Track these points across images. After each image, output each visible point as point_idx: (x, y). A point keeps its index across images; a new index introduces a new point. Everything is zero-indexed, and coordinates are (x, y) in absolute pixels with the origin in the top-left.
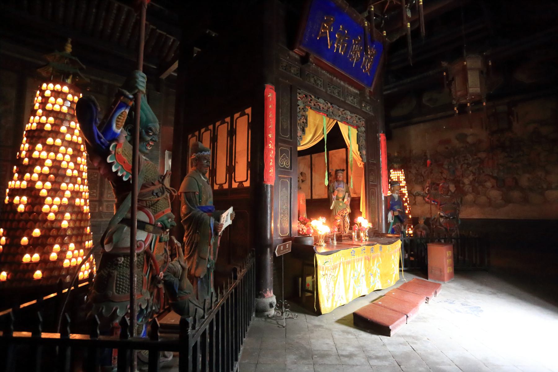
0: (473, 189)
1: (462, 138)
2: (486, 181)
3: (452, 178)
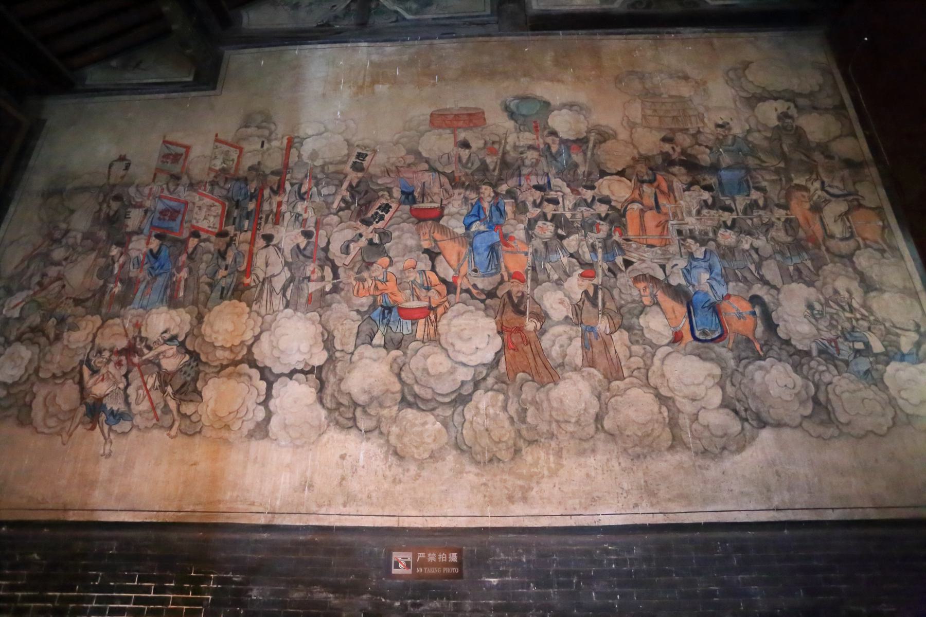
0: (586, 346)
1: (528, 113)
2: (643, 310)
3: (484, 283)
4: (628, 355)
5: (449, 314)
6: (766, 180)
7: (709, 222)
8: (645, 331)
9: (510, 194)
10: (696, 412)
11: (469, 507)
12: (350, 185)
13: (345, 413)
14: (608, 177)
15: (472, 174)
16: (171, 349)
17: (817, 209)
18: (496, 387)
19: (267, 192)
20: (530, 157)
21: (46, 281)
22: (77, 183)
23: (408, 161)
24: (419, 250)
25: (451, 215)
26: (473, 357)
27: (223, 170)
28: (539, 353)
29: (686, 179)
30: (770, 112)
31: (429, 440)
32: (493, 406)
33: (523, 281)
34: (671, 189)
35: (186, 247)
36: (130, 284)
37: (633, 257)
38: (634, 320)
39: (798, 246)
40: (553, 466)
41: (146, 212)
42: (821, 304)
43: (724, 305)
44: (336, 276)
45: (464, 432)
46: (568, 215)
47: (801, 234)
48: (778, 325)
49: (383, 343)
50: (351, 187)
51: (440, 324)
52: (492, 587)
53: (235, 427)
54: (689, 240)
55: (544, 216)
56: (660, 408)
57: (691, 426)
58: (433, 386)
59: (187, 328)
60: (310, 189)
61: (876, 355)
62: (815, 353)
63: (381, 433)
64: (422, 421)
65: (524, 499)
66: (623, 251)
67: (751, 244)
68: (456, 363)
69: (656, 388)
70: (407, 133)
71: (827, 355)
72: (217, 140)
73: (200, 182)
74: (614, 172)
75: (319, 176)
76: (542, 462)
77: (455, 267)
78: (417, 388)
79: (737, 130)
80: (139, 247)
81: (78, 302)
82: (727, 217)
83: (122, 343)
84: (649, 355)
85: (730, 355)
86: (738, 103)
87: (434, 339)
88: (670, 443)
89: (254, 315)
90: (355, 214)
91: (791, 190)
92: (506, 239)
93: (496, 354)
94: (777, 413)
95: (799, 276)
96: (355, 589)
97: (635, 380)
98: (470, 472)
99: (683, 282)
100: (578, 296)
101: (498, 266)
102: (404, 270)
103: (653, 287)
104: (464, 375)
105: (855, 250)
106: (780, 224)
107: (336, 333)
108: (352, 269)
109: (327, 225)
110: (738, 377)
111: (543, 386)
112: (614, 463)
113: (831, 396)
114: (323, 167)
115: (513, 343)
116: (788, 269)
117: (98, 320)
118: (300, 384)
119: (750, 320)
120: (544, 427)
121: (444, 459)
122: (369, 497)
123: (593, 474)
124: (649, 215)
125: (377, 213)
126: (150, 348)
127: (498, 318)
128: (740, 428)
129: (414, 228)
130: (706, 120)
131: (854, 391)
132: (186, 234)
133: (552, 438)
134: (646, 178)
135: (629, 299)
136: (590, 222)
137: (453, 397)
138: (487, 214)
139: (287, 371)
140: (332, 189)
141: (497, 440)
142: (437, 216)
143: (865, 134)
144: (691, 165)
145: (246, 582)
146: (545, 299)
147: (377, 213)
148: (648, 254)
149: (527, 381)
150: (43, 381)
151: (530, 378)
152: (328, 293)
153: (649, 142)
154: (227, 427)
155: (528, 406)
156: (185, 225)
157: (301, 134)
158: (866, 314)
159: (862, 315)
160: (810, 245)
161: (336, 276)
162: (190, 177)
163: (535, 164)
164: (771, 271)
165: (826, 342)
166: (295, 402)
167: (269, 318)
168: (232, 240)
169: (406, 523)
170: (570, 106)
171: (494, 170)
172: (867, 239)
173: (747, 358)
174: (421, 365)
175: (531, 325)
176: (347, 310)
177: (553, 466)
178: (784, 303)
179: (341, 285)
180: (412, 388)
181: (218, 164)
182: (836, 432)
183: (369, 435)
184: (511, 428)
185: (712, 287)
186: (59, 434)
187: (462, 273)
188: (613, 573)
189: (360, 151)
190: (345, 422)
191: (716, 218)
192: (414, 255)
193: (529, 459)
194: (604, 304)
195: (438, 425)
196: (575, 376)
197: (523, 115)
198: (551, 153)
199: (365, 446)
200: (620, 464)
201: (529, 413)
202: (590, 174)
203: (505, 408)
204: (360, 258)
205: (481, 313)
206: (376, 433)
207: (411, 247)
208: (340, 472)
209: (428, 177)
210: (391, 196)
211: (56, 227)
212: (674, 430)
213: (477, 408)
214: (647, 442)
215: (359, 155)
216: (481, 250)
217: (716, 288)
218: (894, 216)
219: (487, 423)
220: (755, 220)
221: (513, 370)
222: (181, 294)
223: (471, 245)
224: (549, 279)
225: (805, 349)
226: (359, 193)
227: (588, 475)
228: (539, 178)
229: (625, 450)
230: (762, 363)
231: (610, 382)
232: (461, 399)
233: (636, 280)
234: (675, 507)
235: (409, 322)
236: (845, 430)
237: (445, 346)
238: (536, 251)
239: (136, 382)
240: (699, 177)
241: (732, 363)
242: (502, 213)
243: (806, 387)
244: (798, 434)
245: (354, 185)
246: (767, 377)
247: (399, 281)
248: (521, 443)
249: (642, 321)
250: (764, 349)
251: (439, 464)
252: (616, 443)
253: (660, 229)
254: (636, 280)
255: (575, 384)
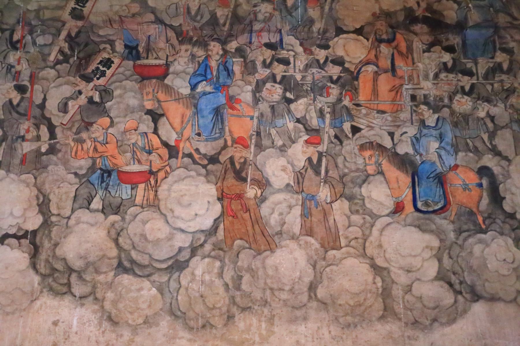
0: (306, 214)
2: (366, 179)
3: (207, 148)
4: (347, 224)
5: (170, 179)
6: (515, 41)
7: (446, 88)
8: (367, 201)
9: (240, 52)
10: (409, 283)
12: (69, 35)
14: (345, 36)
15: (201, 28)
18: (213, 254)
20: (263, 11)
24: (141, 111)
25: (177, 74)
26: (191, 224)
28: (257, 221)
29: (428, 39)
31: (144, 306)
32: (209, 273)
33: (247, 147)
34: (410, 49)
37: (361, 123)
38: (356, 190)
40: (264, 332)
43: (451, 175)
44: (52, 135)
45: (179, 298)
46: (298, 77)
49: (101, 208)
50: (69, 38)
51: (160, 189)
54: (423, 107)
55: (273, 78)
56: (375, 278)
57: (403, 298)
58: (151, 252)
60: (23, 37)
63: (96, 299)
64: (138, 287)
66: (351, 117)
67: (488, 113)
68: (175, 229)
69: (372, 259)
74: (352, 29)
76: (253, 329)
77: (178, 129)
78: (134, 254)
82: (466, 82)
84: (368, 225)
85: (451, 227)
87: (154, 204)
88: (381, 313)
90: (74, 69)
93: (215, 220)
94: (492, 287)
97: (352, 250)
98: (183, 337)
99: (411, 151)
100: (301, 163)
101: (222, 129)
102: (125, 132)
103: (379, 155)
104: (182, 241)
107: (51, 197)
108: (70, 129)
109: (43, 79)
110: (456, 250)
111: (260, 254)
114: (37, 11)
115: (232, 210)
118: (12, 249)
119: (475, 193)
120: (258, 295)
121: (157, 325)
123: (303, 341)
124: (383, 78)
125: (98, 68)
127: (219, 184)
128: (452, 301)
129: (137, 86)
133: (265, 306)
134: (384, 37)
135: (353, 167)
136: (320, 84)
137: (170, 263)
138: (215, 73)
140: (49, 39)
141: (211, 306)
142: (162, 73)
144: (435, 23)
146: (267, 166)
147: (98, 68)
148: (377, 121)
149: (244, 248)
151: (247, 245)
152: (44, 154)
155: (244, 273)
161: (52, 135)
163: (268, 19)
164: (504, 142)
166: (7, 268)
171: (224, 25)
173: (467, 231)
174: (139, 231)
175: (251, 192)
176: (65, 172)
177: (264, 332)
179: (58, 146)
180: (129, 254)
183: (84, 301)
184: (225, 294)
185: (440, 156)
187: (186, 136)
190: (60, 288)
191: (454, 83)
192: (137, 116)
193: (242, 325)
194: (327, 172)
195: (154, 291)
196: (293, 245)
198: (286, 6)
199: (79, 311)
200: (330, 332)
202: (325, 31)
203: (221, 275)
204: (78, 117)
205: (203, 179)
206: (91, 298)
207: (134, 108)
208: (52, 338)
209: (153, 30)
210: (113, 50)
213: (193, 274)
214: (358, 311)
216: (206, 113)
217: (444, 157)
219: (202, 289)
220: (496, 85)
221: (230, 238)
223: (196, 106)
224: (273, 145)
226: (78, 45)
227: (298, 342)
228: (272, 34)
229: (336, 318)
230: (483, 236)
232: (178, 265)
233: (362, 147)
235: (129, 186)
237: (164, 212)
238: (262, 115)
240: (442, 37)
241: (452, 236)
242: (230, 73)
244: (511, 309)
245: (73, 35)
246: (487, 250)
247: (119, 144)
248: (234, 309)
249: (364, 190)
250: (486, 223)
251: (153, 330)
253: (393, 93)
254: (362, 147)
255: (291, 253)
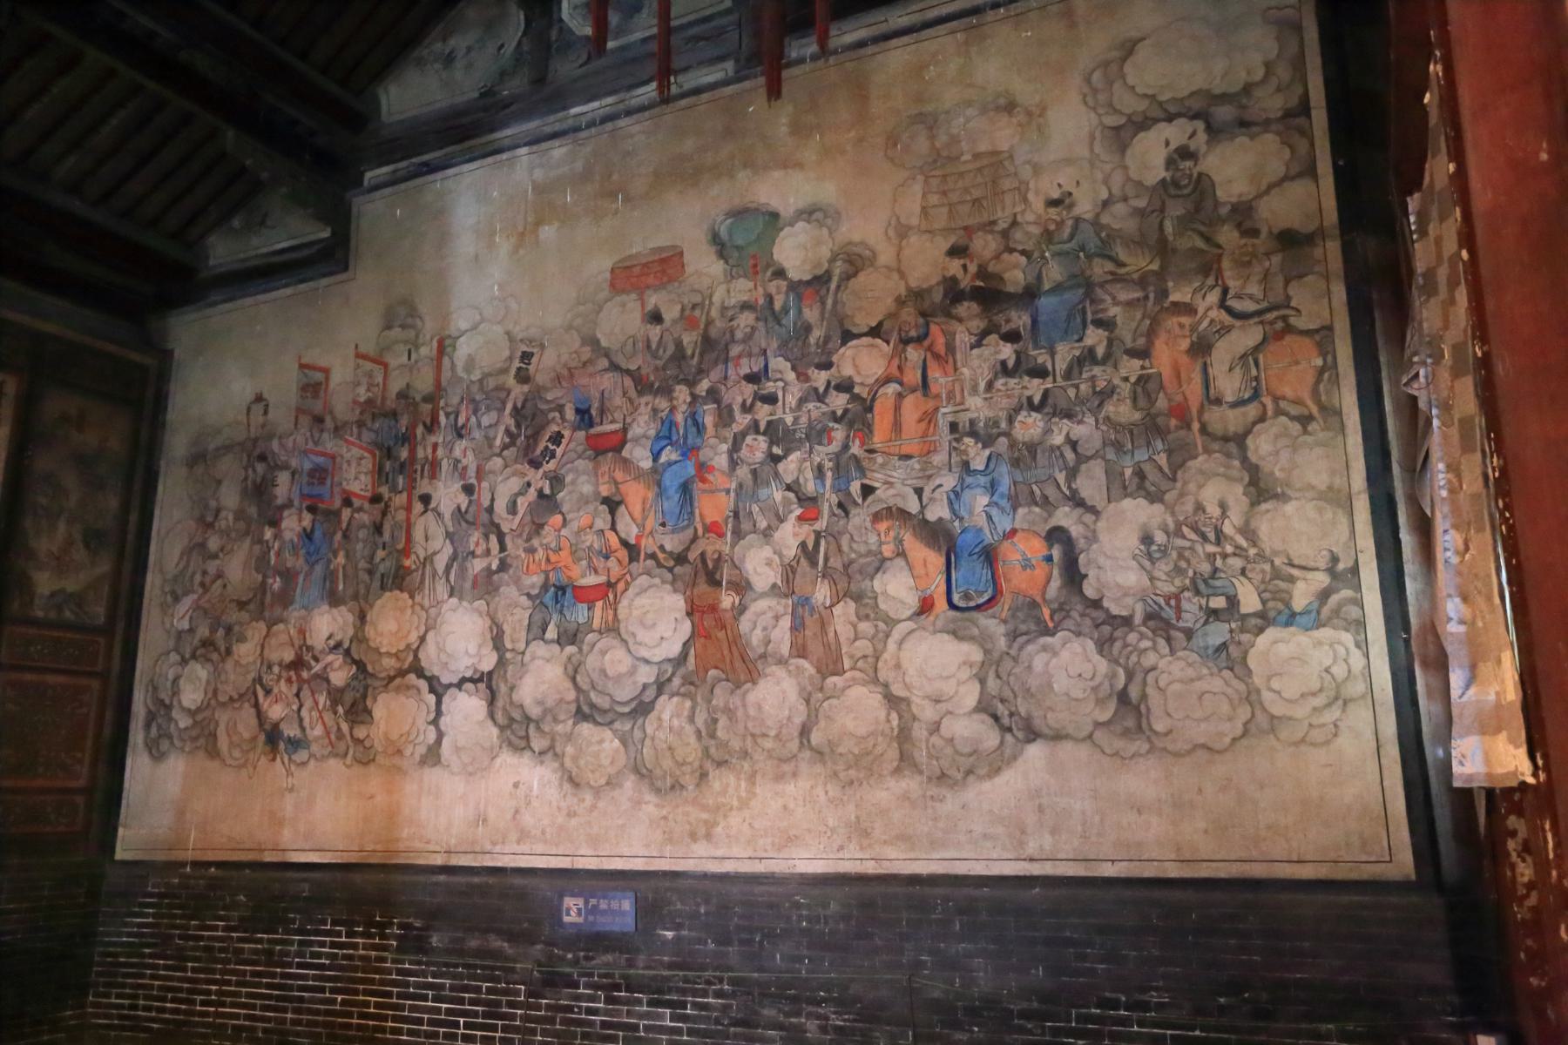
0: (797, 627)
1: (745, 239)
2: (881, 564)
3: (672, 543)
11: (647, 846)
13: (517, 729)
14: (855, 342)
15: (664, 368)
16: (337, 659)
17: (1201, 348)
18: (682, 690)
19: (420, 430)
21: (208, 580)
22: (218, 441)
23: (584, 358)
25: (636, 440)
26: (656, 651)
27: (370, 402)
28: (736, 642)
29: (977, 324)
30: (1151, 154)
32: (678, 716)
33: (721, 535)
34: (950, 348)
35: (340, 522)
36: (288, 576)
37: (876, 479)
39: (1152, 428)
41: (293, 474)
42: (1167, 533)
44: (503, 548)
46: (789, 420)
47: (1162, 403)
48: (1086, 576)
50: (516, 412)
52: (665, 942)
53: (408, 752)
54: (968, 440)
57: (927, 741)
59: (351, 632)
60: (468, 420)
61: (1244, 617)
62: (1138, 619)
63: (556, 755)
65: (708, 836)
69: (886, 686)
70: (582, 308)
71: (1160, 622)
72: (358, 356)
73: (346, 423)
75: (478, 398)
76: (731, 791)
79: (1084, 207)
80: (293, 524)
81: (242, 605)
82: (1035, 388)
83: (289, 656)
84: (881, 635)
86: (1097, 149)
87: (612, 629)
88: (895, 764)
89: (417, 608)
91: (1163, 309)
92: (703, 469)
94: (1057, 719)
95: (1140, 485)
96: (529, 938)
97: (857, 674)
99: (946, 514)
100: (791, 551)
104: (646, 675)
105: (1254, 424)
106: (1125, 389)
107: (505, 627)
108: (520, 535)
110: (1007, 664)
112: (820, 791)
113: (1150, 691)
114: (481, 381)
116: (1122, 474)
117: (262, 626)
120: (736, 744)
121: (621, 786)
122: (543, 832)
123: (792, 805)
124: (909, 401)
126: (317, 660)
129: (591, 465)
130: (1031, 196)
131: (1192, 680)
132: (338, 503)
137: (633, 705)
139: (455, 681)
140: (494, 415)
143: (1335, 164)
144: (990, 295)
145: (426, 928)
148: (899, 472)
149: (720, 680)
150: (223, 705)
153: (927, 262)
154: (399, 752)
156: (337, 490)
157: (453, 331)
158: (1244, 544)
159: (1237, 547)
160: (1173, 422)
161: (503, 548)
162: (334, 418)
164: (1091, 484)
165: (1161, 601)
167: (433, 611)
168: (387, 506)
169: (581, 864)
170: (808, 213)
172: (1284, 398)
178: (1104, 537)
179: (509, 560)
181: (363, 394)
182: (1146, 746)
185: (990, 517)
186: (244, 766)
188: (803, 931)
189: (525, 349)
192: (591, 507)
193: (717, 785)
194: (826, 559)
196: (779, 671)
197: (738, 248)
198: (772, 310)
201: (720, 724)
202: (827, 339)
203: (691, 719)
204: (528, 518)
205: (668, 587)
206: (550, 754)
209: (608, 381)
211: (206, 506)
212: (905, 743)
213: (660, 719)
215: (526, 357)
218: (1349, 341)
219: (671, 739)
220: (1083, 387)
222: (341, 587)
225: (1124, 613)
227: (785, 807)
229: (835, 774)
230: (1049, 639)
231: (824, 678)
232: (642, 708)
233: (877, 517)
234: (891, 852)
235: (585, 606)
236: (1159, 743)
237: (625, 636)
238: (740, 486)
239: (308, 703)
240: (1000, 319)
241: (1002, 643)
242: (700, 429)
243: (1114, 676)
244: (1083, 751)
248: (708, 765)
250: (1056, 618)
251: (616, 793)
252: (824, 763)
253: (923, 425)
254: (877, 517)
